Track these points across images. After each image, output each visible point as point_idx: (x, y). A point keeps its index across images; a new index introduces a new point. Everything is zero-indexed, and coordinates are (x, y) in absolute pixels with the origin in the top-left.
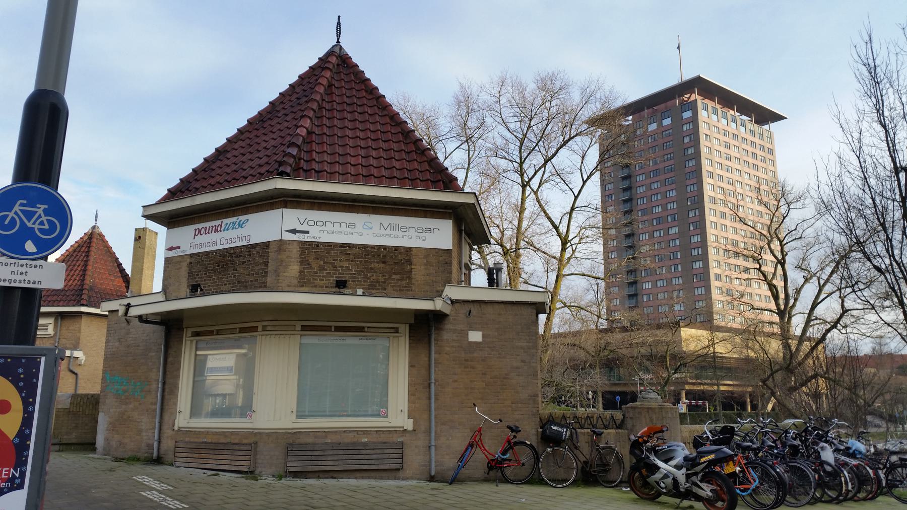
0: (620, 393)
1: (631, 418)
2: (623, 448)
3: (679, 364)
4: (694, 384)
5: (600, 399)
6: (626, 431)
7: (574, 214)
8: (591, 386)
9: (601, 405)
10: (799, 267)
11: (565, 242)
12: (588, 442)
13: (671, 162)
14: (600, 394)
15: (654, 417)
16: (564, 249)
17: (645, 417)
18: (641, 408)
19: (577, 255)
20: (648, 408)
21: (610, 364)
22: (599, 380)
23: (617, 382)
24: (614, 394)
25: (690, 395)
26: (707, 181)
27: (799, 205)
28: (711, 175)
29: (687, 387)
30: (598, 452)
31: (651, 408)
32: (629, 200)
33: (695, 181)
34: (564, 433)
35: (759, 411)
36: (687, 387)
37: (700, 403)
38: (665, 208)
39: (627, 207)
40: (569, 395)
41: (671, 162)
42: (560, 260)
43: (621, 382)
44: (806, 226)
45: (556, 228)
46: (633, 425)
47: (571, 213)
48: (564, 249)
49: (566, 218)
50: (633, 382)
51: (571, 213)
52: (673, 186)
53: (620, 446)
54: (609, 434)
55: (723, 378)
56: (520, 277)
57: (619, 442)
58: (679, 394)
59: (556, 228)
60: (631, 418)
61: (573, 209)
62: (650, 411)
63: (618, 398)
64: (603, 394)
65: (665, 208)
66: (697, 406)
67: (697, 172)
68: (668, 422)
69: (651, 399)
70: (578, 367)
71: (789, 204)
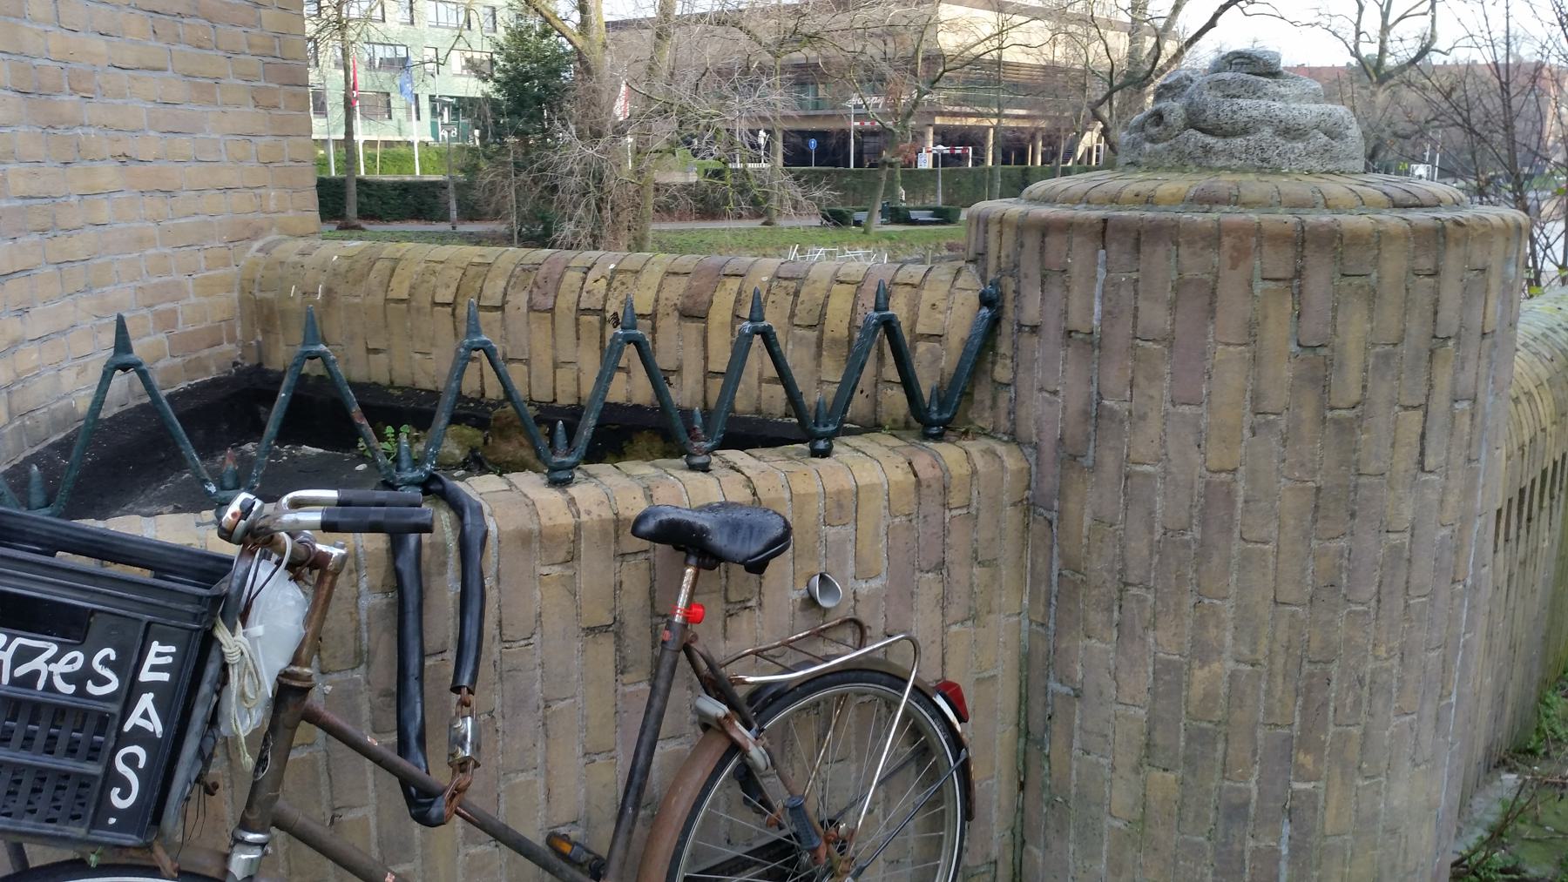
0: (813, 134)
1: (1087, 343)
2: (973, 617)
3: (941, 70)
4: (954, 115)
5: (779, 145)
6: (1012, 459)
8: (764, 119)
9: (780, 159)
12: (614, 629)
14: (780, 135)
15: (1355, 329)
17: (1252, 331)
18: (1214, 237)
20: (1302, 241)
21: (804, 76)
22: (778, 100)
23: (812, 113)
24: (805, 135)
25: (943, 136)
29: (938, 121)
30: (718, 747)
31: (1333, 241)
34: (146, 715)
35: (1058, 164)
36: (938, 121)
37: (958, 151)
40: (710, 133)
43: (818, 112)
46: (1096, 415)
50: (841, 112)
53: (944, 602)
54: (845, 506)
55: (1009, 104)
56: (974, 472)
57: (940, 566)
58: (923, 134)
60: (1087, 343)
62: (1319, 278)
63: (813, 143)
64: (786, 134)
66: (952, 155)
68: (1467, 378)
69: (1290, 131)
70: (747, 76)
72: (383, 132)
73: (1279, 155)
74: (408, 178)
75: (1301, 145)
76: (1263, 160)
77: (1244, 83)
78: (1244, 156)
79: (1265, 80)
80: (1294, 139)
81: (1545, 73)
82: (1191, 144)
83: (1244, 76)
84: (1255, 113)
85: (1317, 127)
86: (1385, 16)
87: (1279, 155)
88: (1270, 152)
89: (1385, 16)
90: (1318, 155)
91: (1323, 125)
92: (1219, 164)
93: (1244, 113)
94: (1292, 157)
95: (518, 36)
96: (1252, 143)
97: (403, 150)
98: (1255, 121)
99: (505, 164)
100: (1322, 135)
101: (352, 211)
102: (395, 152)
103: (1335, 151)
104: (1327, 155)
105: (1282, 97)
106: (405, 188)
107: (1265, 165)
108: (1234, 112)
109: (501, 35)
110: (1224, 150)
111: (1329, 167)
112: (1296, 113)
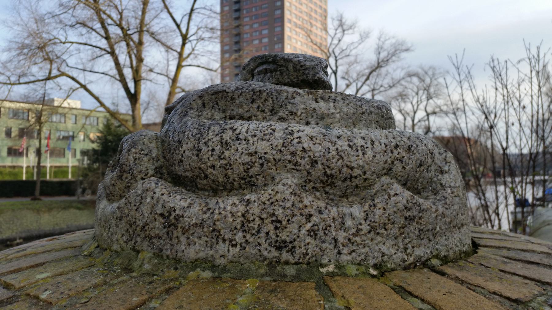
7: (194, 16)
10: (343, 78)
11: (185, 38)
13: (266, 10)
16: (184, 44)
19: (196, 52)
26: (287, 26)
27: (350, 31)
28: (290, 21)
32: (238, 35)
33: (280, 24)
38: (260, 42)
39: (236, 39)
41: (266, 10)
42: (180, 54)
44: (352, 48)
45: (178, 26)
47: (190, 14)
48: (184, 44)
49: (187, 18)
51: (190, 14)
52: (267, 27)
59: (178, 26)
61: (192, 10)
65: (260, 42)
67: (281, 19)
71: (344, 31)
72: (60, 162)
73: (313, 233)
74: (65, 179)
75: (357, 211)
76: (280, 246)
77: (256, 95)
78: (239, 237)
79: (291, 90)
80: (345, 195)
81: (479, 143)
82: (146, 209)
83: (270, 86)
84: (262, 147)
85: (388, 172)
86: (413, 121)
87: (313, 233)
88: (293, 228)
89: (413, 121)
90: (395, 231)
91: (398, 167)
92: (191, 253)
93: (242, 146)
94: (342, 236)
95: (108, 126)
96: (255, 209)
97: (65, 169)
98: (264, 161)
99: (98, 173)
100: (397, 187)
101: (37, 192)
102: (60, 170)
103: (430, 217)
104: (413, 228)
105: (322, 118)
106: (61, 183)
107: (285, 256)
108: (225, 145)
109: (101, 126)
110: (201, 225)
111: (419, 252)
112: (343, 144)
